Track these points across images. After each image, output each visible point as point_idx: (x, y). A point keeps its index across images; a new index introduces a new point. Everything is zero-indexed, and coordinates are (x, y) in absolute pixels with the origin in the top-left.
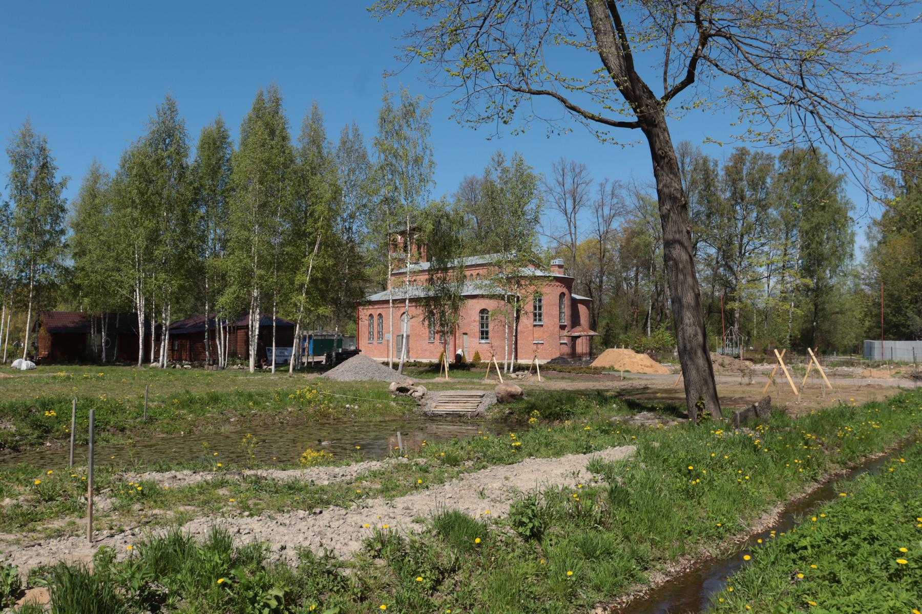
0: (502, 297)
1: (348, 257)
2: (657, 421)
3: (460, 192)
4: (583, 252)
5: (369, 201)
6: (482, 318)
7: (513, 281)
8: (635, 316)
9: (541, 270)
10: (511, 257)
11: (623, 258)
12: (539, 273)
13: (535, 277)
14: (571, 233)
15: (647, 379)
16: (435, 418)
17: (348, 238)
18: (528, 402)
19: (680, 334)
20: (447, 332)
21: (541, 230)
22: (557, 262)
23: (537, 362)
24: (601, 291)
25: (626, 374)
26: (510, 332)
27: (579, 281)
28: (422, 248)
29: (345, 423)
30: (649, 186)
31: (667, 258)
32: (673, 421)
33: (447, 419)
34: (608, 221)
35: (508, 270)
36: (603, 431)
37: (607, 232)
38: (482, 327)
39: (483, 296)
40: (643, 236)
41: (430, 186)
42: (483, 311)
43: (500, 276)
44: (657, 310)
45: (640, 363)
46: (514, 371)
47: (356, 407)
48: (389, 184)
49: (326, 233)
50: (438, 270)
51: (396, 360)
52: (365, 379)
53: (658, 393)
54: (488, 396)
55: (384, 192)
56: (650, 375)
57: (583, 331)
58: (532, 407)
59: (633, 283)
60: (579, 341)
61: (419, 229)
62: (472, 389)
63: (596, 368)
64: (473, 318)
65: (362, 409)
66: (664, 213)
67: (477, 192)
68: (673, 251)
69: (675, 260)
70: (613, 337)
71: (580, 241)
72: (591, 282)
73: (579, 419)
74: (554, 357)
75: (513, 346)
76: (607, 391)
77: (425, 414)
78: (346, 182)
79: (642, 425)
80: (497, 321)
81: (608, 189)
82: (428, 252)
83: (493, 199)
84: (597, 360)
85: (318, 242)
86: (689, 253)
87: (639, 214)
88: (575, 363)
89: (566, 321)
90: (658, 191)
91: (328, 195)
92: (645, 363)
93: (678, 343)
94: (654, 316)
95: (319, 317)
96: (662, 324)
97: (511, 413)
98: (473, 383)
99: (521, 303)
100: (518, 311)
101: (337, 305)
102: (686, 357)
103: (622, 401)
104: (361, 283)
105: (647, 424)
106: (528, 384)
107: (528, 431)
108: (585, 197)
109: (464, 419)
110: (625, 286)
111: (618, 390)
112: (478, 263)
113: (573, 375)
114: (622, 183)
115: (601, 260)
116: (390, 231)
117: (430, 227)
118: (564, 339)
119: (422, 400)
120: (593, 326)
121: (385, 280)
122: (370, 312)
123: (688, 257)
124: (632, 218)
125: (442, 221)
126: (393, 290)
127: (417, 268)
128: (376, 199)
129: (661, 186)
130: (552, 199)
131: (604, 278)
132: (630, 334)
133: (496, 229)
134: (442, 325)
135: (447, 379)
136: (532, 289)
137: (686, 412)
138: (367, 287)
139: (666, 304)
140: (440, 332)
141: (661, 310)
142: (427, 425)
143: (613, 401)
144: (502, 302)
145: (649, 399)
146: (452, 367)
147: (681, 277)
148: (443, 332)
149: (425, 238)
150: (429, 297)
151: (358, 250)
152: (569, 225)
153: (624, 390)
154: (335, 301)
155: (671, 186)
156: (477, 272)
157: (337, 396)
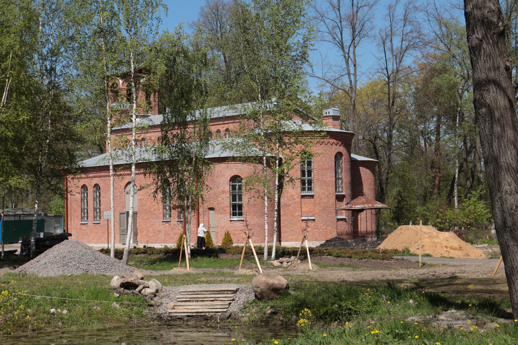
0: (259, 160)
1: (51, 109)
2: (469, 322)
3: (201, 19)
4: (365, 98)
5: (78, 32)
6: (234, 187)
7: (273, 138)
8: (437, 182)
9: (310, 124)
10: (270, 106)
11: (419, 106)
12: (307, 127)
13: (303, 132)
14: (349, 74)
15: (454, 266)
16: (172, 323)
17: (50, 83)
18: (296, 298)
19: (498, 205)
20: (188, 207)
21: (309, 70)
22: (331, 112)
23: (307, 245)
24: (390, 149)
25: (427, 258)
26: (271, 205)
27: (360, 137)
28: (152, 96)
29: (49, 334)
30: (454, 6)
31: (478, 103)
32: (492, 322)
33: (189, 323)
34: (399, 56)
35: (267, 123)
36: (396, 336)
37: (398, 71)
38: (234, 199)
39: (234, 159)
40: (447, 75)
41: (160, 11)
42: (235, 179)
43: (257, 131)
44: (466, 173)
45: (445, 243)
46: (277, 257)
47: (65, 312)
48: (104, 10)
49: (18, 76)
50: (174, 124)
51: (119, 246)
52: (76, 273)
53: (469, 284)
54: (243, 291)
55: (97, 19)
56: (459, 260)
57: (367, 202)
58: (301, 305)
59: (433, 138)
60: (362, 216)
61: (147, 71)
62: (221, 282)
63: (385, 252)
64: (221, 189)
65: (73, 313)
66: (474, 44)
67: (224, 20)
68: (486, 95)
69: (488, 107)
70: (407, 210)
71: (362, 83)
72: (376, 137)
73: (364, 320)
74: (329, 237)
75: (276, 224)
76: (401, 281)
77: (160, 318)
78: (44, 5)
79: (450, 327)
80: (253, 191)
81: (399, 12)
82: (160, 100)
83: (245, 30)
84: (386, 240)
85: (7, 88)
86: (508, 97)
87: (442, 46)
88: (357, 245)
89: (345, 191)
90: (466, 14)
91: (19, 23)
92: (450, 244)
93: (494, 216)
94: (463, 181)
95: (10, 190)
96: (473, 192)
97: (274, 313)
98: (223, 274)
99: (285, 167)
100: (281, 178)
101: (36, 174)
102: (507, 236)
103: (421, 295)
104: (70, 144)
105: (456, 326)
106: (295, 273)
107: (296, 336)
108: (368, 25)
109: (210, 323)
110: (422, 142)
111: (416, 281)
112: (228, 115)
113: (355, 260)
114: (417, 5)
115: (389, 108)
116: (108, 74)
117: (161, 68)
118: (342, 214)
119: (156, 299)
120: (380, 196)
121: (103, 139)
122: (83, 182)
123: (507, 102)
124: (432, 51)
125: (178, 60)
126: (113, 153)
127: (146, 122)
128: (89, 30)
129: (470, 7)
130: (323, 28)
131: (394, 132)
132: (430, 206)
133: (250, 70)
134: (180, 198)
135: (188, 269)
136: (298, 148)
137: (509, 311)
138: (78, 149)
139: (478, 165)
140: (178, 207)
141: (472, 173)
142: (162, 332)
143: (408, 295)
144: (260, 167)
145: (458, 292)
146: (194, 253)
147: (497, 129)
148: (181, 207)
149: (155, 80)
150: (163, 161)
151: (65, 98)
152: (347, 63)
153: (423, 280)
154: (33, 169)
155: (485, 7)
156: (226, 126)
157: (38, 297)
